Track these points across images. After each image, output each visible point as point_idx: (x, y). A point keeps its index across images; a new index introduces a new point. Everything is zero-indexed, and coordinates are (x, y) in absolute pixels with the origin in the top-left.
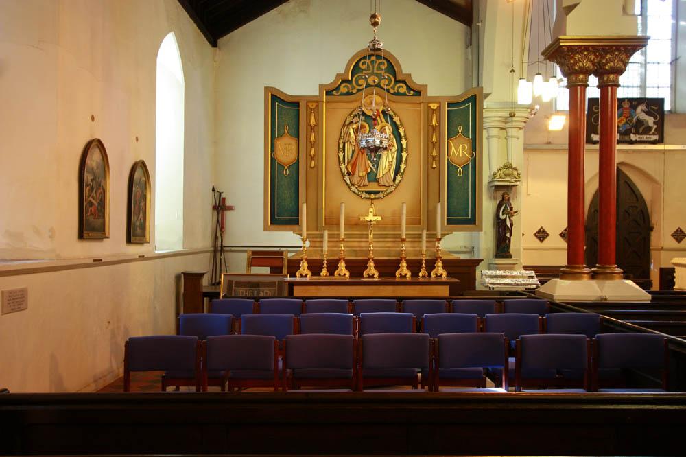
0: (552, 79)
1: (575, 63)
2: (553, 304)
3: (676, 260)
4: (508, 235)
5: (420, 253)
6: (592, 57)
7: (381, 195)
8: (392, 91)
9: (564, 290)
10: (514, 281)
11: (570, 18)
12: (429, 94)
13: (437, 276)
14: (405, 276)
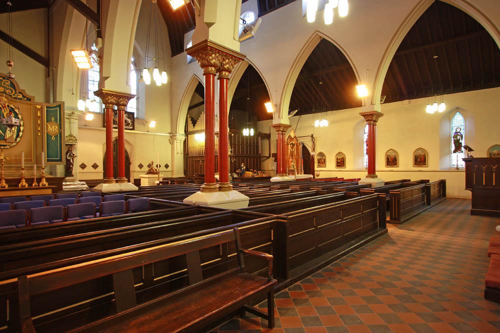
0: (87, 100)
1: (108, 100)
2: (103, 193)
3: (141, 176)
4: (71, 166)
5: (33, 175)
6: (115, 98)
7: (8, 147)
8: (13, 96)
9: (106, 187)
10: (76, 186)
11: (106, 82)
12: (36, 101)
13: (43, 185)
14: (25, 186)
